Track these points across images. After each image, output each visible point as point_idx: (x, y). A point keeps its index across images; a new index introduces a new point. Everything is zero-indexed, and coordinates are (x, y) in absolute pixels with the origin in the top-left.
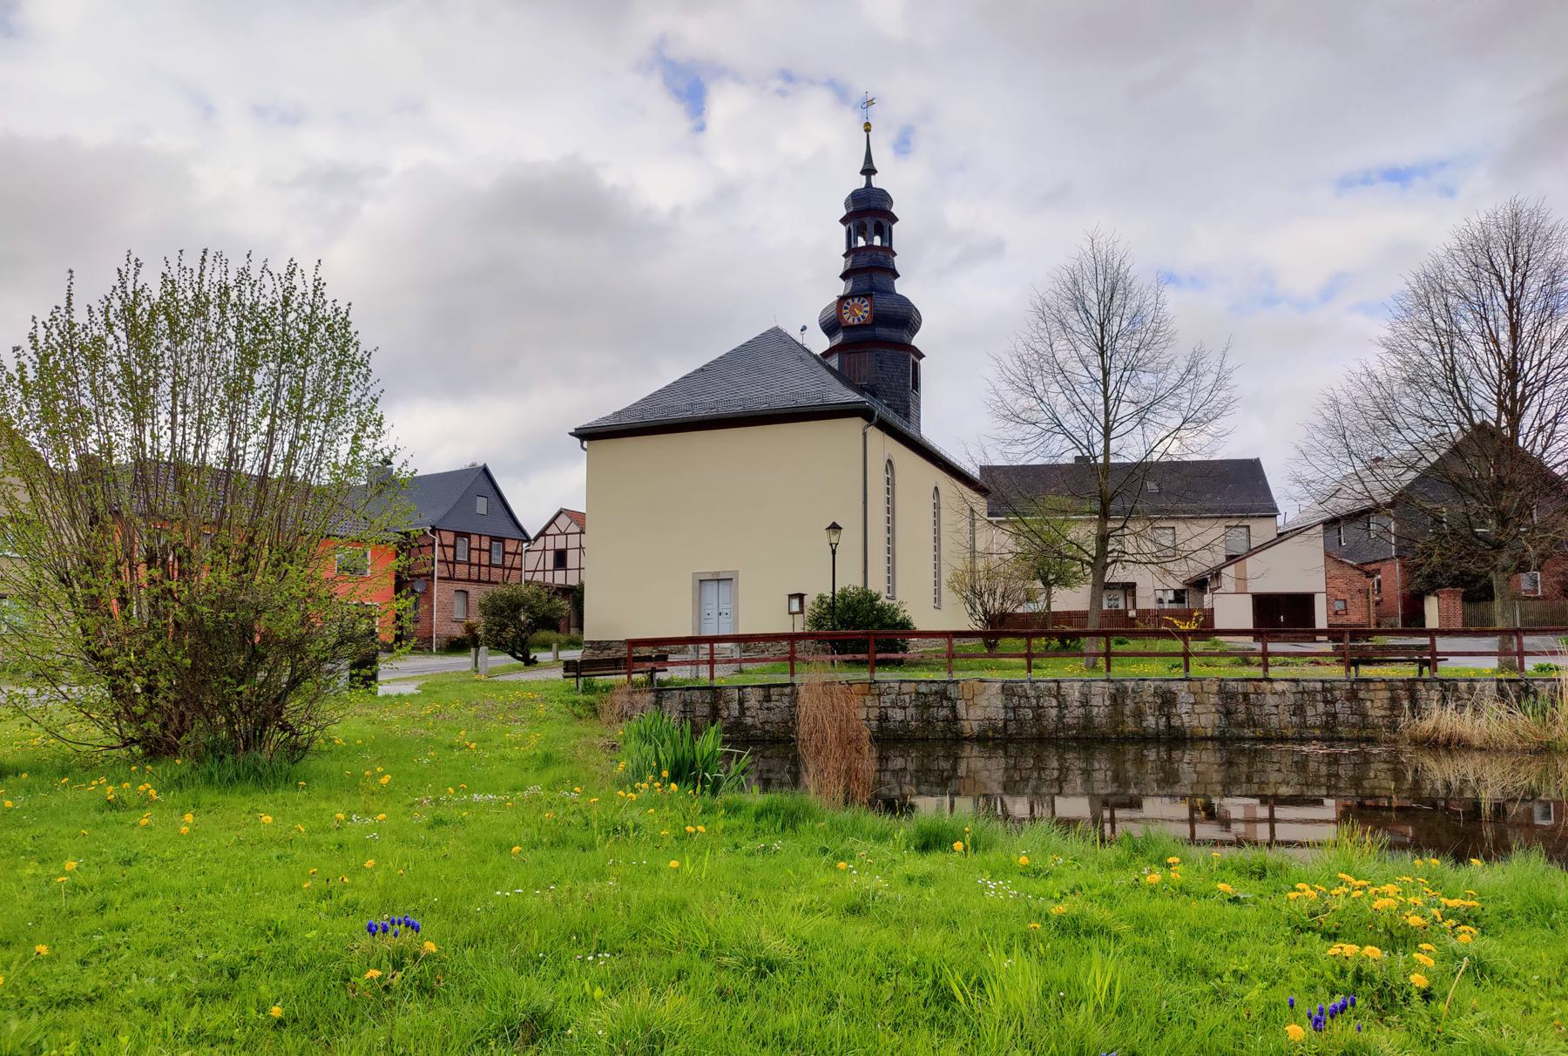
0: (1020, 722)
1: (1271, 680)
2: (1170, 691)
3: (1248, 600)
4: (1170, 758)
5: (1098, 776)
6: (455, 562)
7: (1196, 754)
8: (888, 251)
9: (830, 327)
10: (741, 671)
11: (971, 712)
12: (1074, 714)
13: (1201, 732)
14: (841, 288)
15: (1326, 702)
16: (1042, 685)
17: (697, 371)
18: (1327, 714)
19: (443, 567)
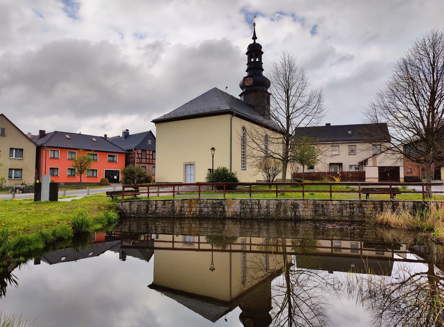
1: (331, 200)
2: (297, 204)
3: (377, 169)
4: (295, 225)
5: (271, 231)
7: (304, 225)
8: (260, 63)
9: (242, 87)
11: (229, 209)
13: (306, 218)
14: (246, 74)
15: (350, 208)
16: (254, 201)
17: (190, 102)
18: (350, 212)
19: (138, 160)
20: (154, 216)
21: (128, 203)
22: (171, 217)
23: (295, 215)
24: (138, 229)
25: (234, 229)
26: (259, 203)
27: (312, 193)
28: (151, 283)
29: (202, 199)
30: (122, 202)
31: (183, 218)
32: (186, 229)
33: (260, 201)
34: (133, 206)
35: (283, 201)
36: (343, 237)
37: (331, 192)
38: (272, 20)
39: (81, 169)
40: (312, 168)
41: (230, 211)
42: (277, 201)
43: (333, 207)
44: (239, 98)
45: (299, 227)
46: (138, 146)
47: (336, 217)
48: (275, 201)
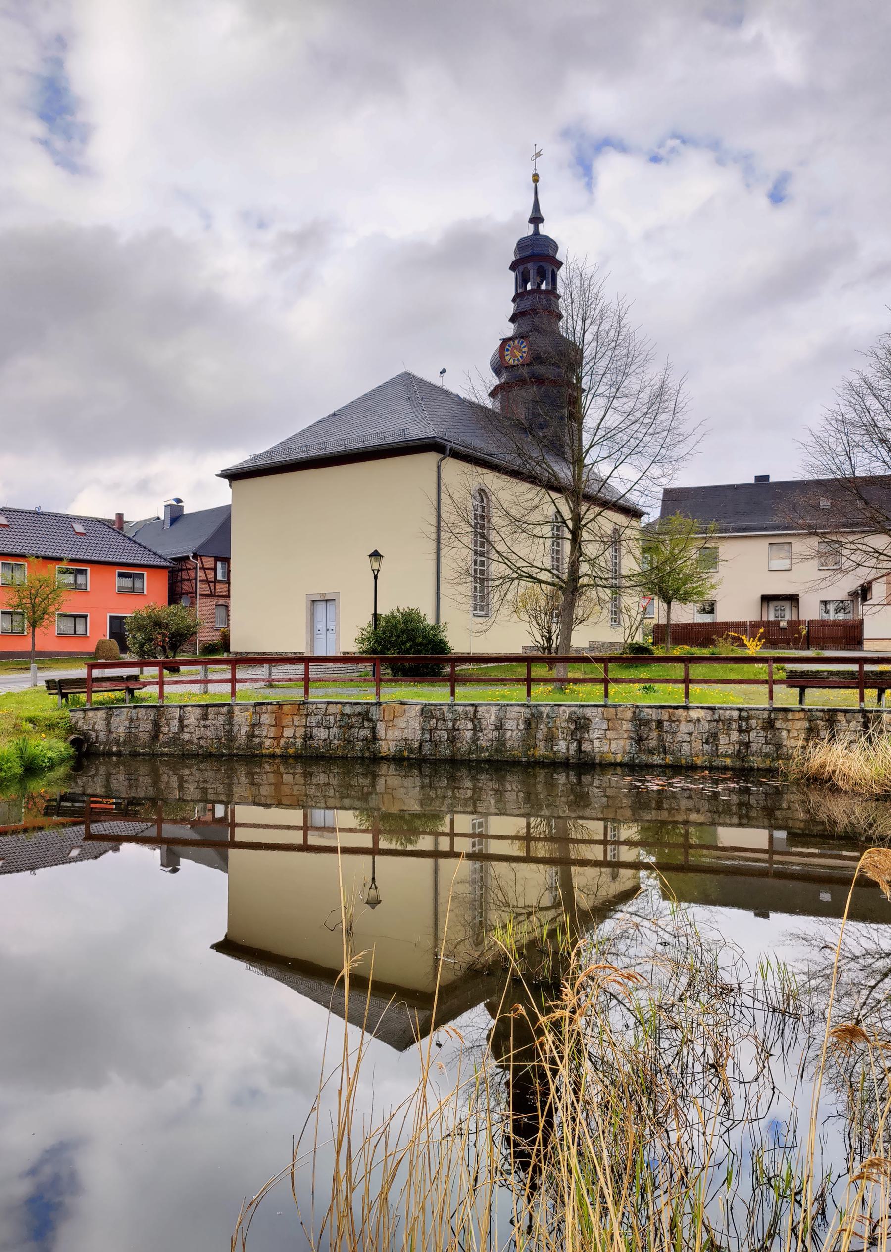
0: (435, 744)
4: (579, 781)
6: (216, 581)
8: (552, 292)
9: (498, 368)
10: (271, 684)
11: (390, 733)
12: (487, 737)
13: (611, 758)
14: (510, 330)
15: (740, 731)
16: (460, 709)
17: (330, 416)
18: (740, 743)
19: (205, 586)
20: (174, 749)
21: (101, 714)
22: (223, 755)
23: (579, 750)
24: (130, 786)
25: (403, 790)
26: (475, 716)
27: (647, 685)
28: (222, 938)
29: (313, 703)
30: (85, 711)
31: (257, 756)
32: (267, 788)
33: (480, 709)
34: (115, 721)
35: (545, 710)
36: (716, 816)
37: (687, 681)
38: (655, 159)
39: (34, 613)
40: (710, 608)
41: (390, 740)
42: (528, 710)
43: (690, 727)
44: (488, 403)
45: (591, 784)
46: (203, 546)
47: (697, 756)
48: (522, 709)
